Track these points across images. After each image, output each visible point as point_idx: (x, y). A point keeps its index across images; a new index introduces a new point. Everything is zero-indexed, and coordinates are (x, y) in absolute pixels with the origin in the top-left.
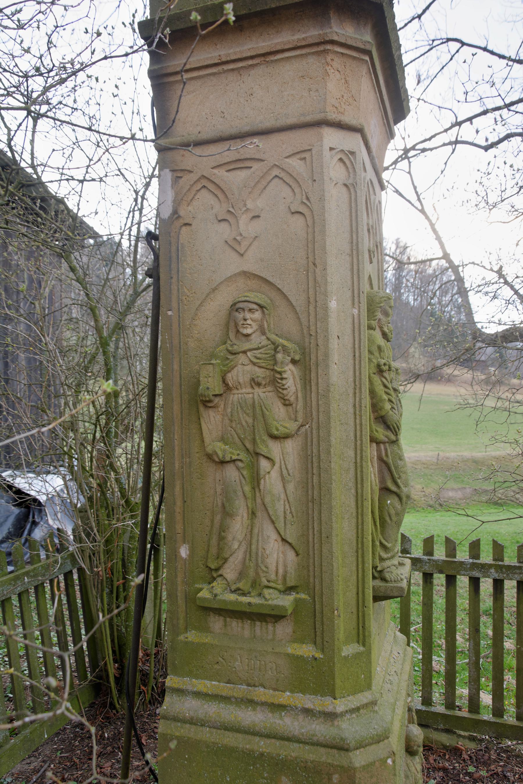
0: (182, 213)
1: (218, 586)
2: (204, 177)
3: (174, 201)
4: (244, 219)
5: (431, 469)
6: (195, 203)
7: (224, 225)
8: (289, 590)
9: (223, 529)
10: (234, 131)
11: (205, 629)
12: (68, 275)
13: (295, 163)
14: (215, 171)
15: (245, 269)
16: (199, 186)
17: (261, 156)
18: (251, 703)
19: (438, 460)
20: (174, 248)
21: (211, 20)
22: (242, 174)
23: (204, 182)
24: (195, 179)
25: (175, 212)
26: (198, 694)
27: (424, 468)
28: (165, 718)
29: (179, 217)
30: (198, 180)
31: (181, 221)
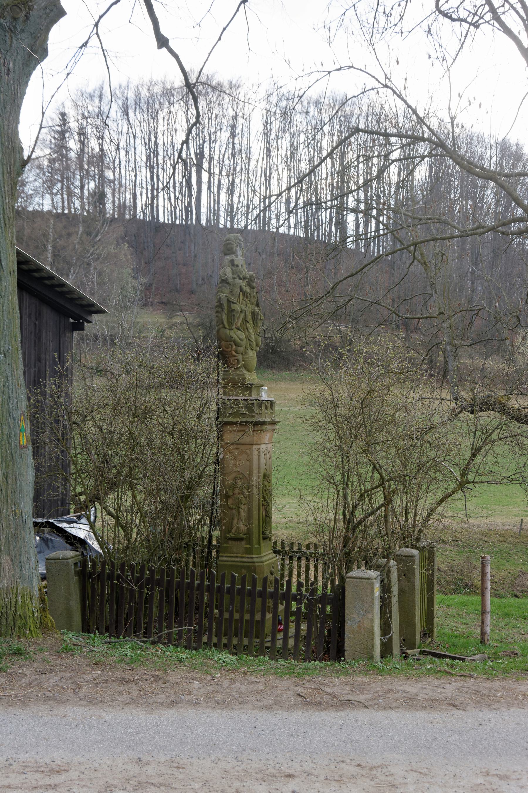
1: (231, 534)
5: (510, 543)
8: (245, 534)
9: (232, 522)
11: (228, 544)
13: (248, 451)
18: (237, 557)
19: (521, 529)
26: (226, 556)
27: (499, 541)
28: (358, 125)
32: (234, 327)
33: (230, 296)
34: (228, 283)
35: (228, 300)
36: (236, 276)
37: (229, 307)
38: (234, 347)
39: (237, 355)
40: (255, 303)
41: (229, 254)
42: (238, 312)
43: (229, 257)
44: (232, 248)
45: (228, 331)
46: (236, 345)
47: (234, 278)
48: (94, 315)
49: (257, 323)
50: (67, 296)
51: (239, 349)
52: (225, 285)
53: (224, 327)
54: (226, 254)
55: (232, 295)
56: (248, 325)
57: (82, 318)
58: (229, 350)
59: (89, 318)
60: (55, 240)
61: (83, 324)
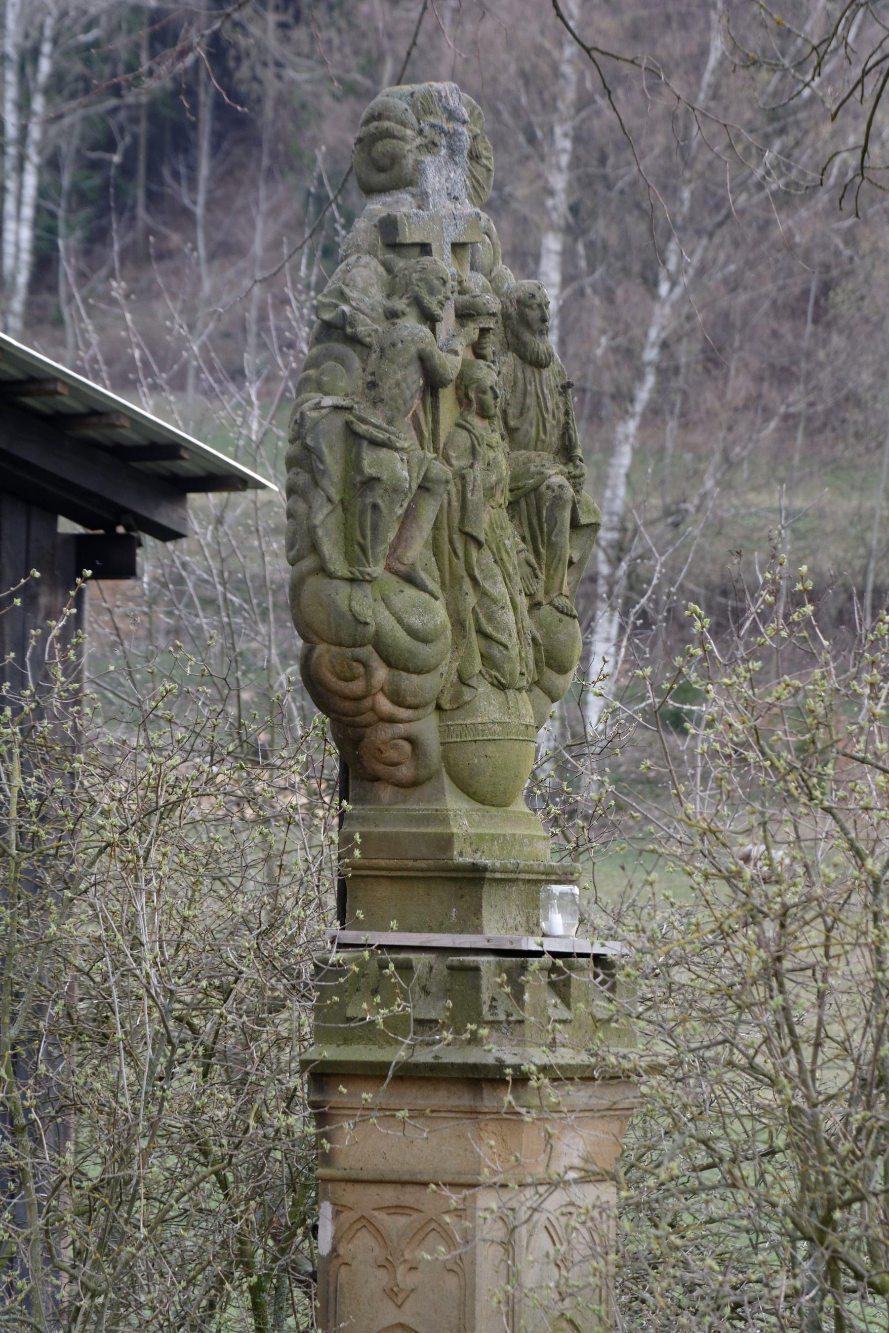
0: (341, 1251)
2: (363, 1217)
3: (334, 1238)
4: (401, 1270)
6: (355, 1241)
7: (382, 1270)
10: (394, 1177)
12: (505, 1195)
14: (376, 1213)
15: (402, 1321)
16: (359, 1225)
17: (420, 1207)
20: (332, 1288)
21: (571, 350)
22: (402, 1221)
23: (365, 1223)
24: (355, 1218)
25: (334, 1250)
29: (338, 1256)
30: (359, 1220)
31: (341, 1260)
32: (377, 570)
33: (363, 409)
34: (354, 341)
35: (348, 425)
36: (400, 304)
37: (353, 464)
38: (381, 673)
39: (402, 713)
40: (553, 438)
41: (383, 190)
42: (396, 490)
43: (377, 207)
44: (395, 159)
45: (342, 593)
46: (389, 663)
47: (392, 315)
48: (195, 499)
49: (551, 546)
50: (30, 401)
51: (411, 682)
52: (340, 348)
53: (323, 570)
54: (370, 190)
55: (376, 402)
56: (483, 559)
57: (120, 513)
58: (357, 686)
59: (165, 517)
60: (584, 102)
61: (131, 544)
